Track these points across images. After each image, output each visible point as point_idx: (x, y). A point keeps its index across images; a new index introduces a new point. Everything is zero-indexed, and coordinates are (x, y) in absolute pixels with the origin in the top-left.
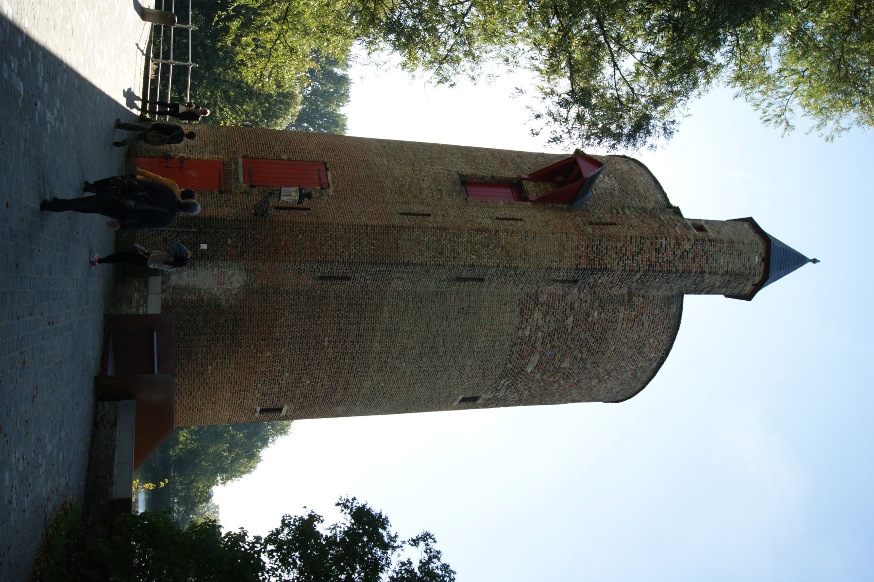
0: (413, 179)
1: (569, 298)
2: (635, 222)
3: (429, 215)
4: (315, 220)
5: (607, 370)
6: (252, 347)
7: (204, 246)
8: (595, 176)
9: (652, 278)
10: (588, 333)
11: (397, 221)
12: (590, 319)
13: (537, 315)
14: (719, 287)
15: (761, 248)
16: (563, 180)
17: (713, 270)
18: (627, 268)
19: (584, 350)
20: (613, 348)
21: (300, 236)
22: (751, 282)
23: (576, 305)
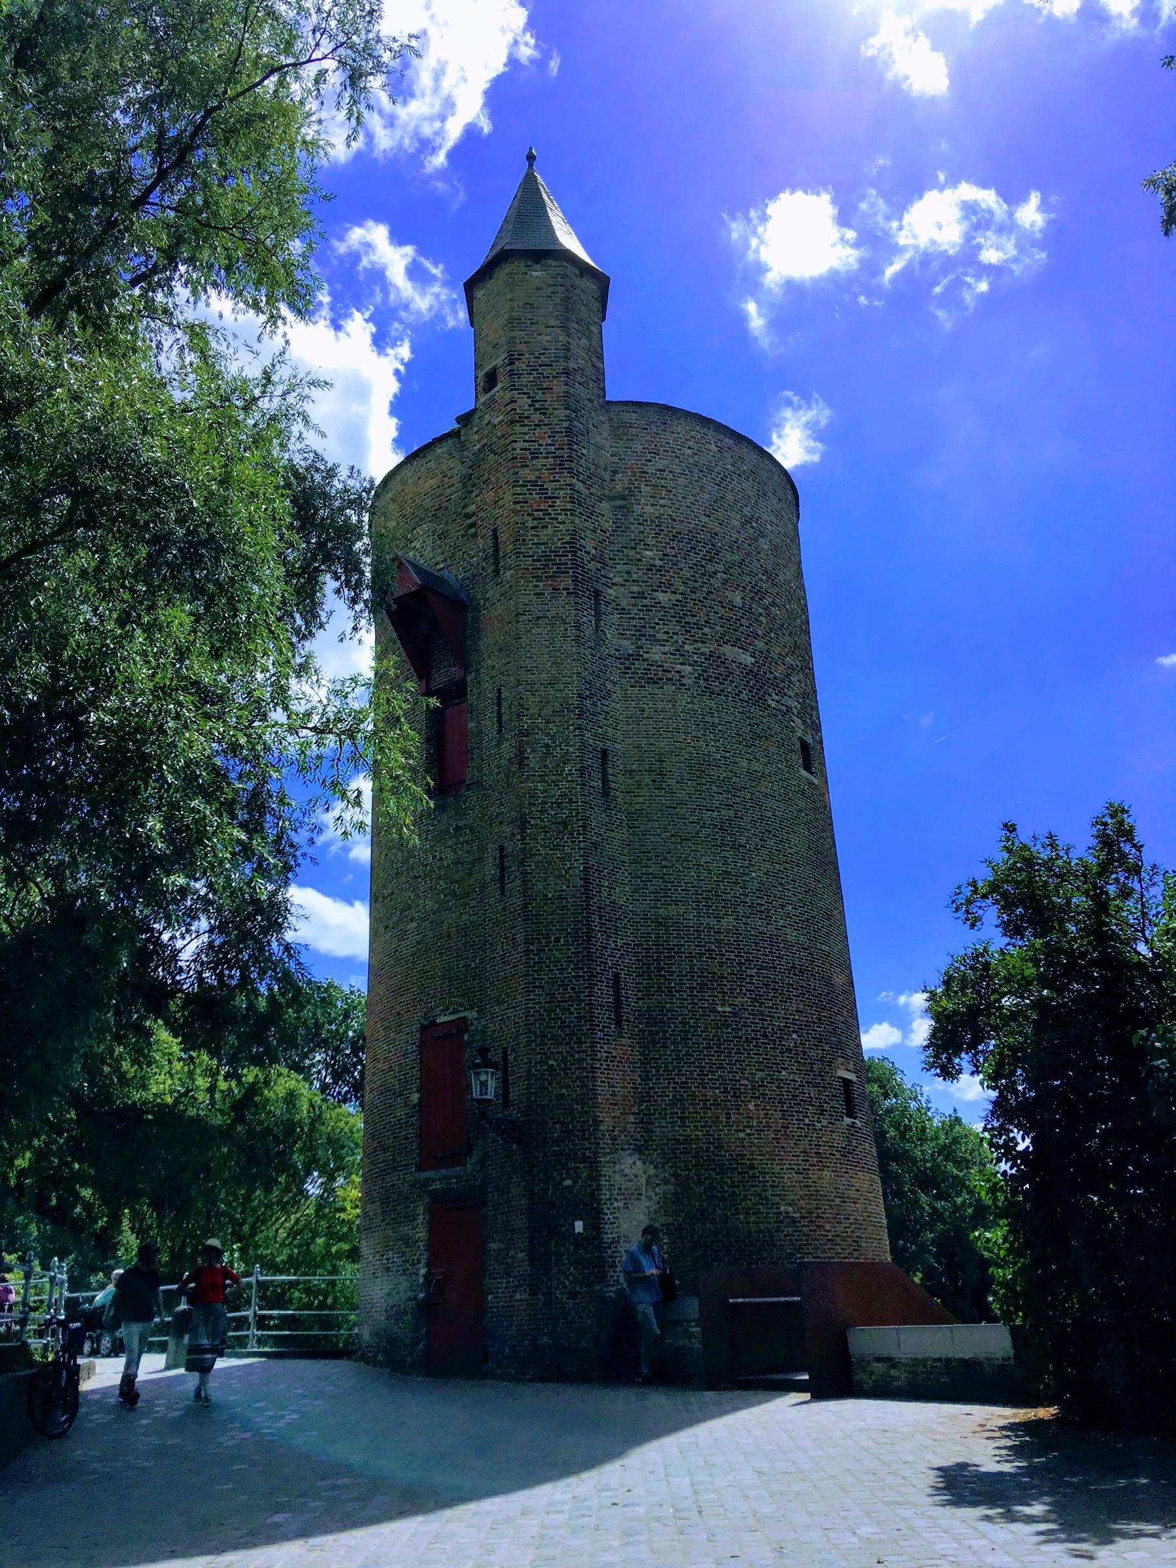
0: (440, 878)
1: (624, 603)
2: (489, 496)
3: (502, 848)
4: (523, 1039)
5: (743, 525)
6: (742, 1135)
7: (579, 1226)
8: (419, 570)
9: (582, 461)
10: (681, 565)
11: (517, 901)
12: (658, 563)
13: (656, 654)
14: (589, 338)
15: (518, 266)
16: (425, 625)
17: (562, 353)
18: (569, 506)
19: (710, 568)
20: (704, 519)
21: (551, 1062)
22: (577, 281)
23: (635, 589)
